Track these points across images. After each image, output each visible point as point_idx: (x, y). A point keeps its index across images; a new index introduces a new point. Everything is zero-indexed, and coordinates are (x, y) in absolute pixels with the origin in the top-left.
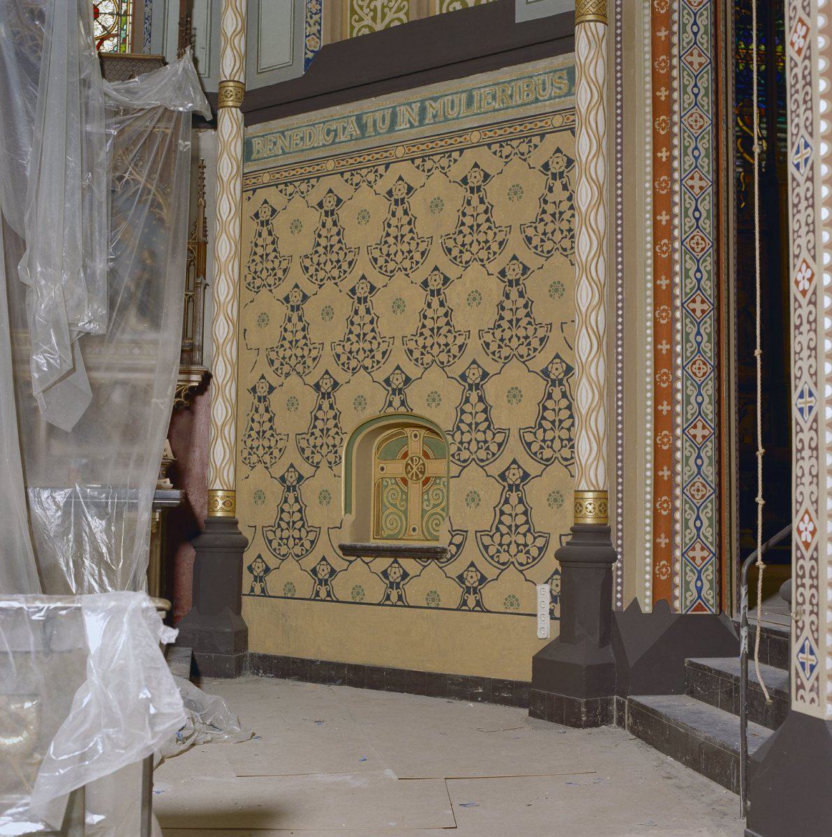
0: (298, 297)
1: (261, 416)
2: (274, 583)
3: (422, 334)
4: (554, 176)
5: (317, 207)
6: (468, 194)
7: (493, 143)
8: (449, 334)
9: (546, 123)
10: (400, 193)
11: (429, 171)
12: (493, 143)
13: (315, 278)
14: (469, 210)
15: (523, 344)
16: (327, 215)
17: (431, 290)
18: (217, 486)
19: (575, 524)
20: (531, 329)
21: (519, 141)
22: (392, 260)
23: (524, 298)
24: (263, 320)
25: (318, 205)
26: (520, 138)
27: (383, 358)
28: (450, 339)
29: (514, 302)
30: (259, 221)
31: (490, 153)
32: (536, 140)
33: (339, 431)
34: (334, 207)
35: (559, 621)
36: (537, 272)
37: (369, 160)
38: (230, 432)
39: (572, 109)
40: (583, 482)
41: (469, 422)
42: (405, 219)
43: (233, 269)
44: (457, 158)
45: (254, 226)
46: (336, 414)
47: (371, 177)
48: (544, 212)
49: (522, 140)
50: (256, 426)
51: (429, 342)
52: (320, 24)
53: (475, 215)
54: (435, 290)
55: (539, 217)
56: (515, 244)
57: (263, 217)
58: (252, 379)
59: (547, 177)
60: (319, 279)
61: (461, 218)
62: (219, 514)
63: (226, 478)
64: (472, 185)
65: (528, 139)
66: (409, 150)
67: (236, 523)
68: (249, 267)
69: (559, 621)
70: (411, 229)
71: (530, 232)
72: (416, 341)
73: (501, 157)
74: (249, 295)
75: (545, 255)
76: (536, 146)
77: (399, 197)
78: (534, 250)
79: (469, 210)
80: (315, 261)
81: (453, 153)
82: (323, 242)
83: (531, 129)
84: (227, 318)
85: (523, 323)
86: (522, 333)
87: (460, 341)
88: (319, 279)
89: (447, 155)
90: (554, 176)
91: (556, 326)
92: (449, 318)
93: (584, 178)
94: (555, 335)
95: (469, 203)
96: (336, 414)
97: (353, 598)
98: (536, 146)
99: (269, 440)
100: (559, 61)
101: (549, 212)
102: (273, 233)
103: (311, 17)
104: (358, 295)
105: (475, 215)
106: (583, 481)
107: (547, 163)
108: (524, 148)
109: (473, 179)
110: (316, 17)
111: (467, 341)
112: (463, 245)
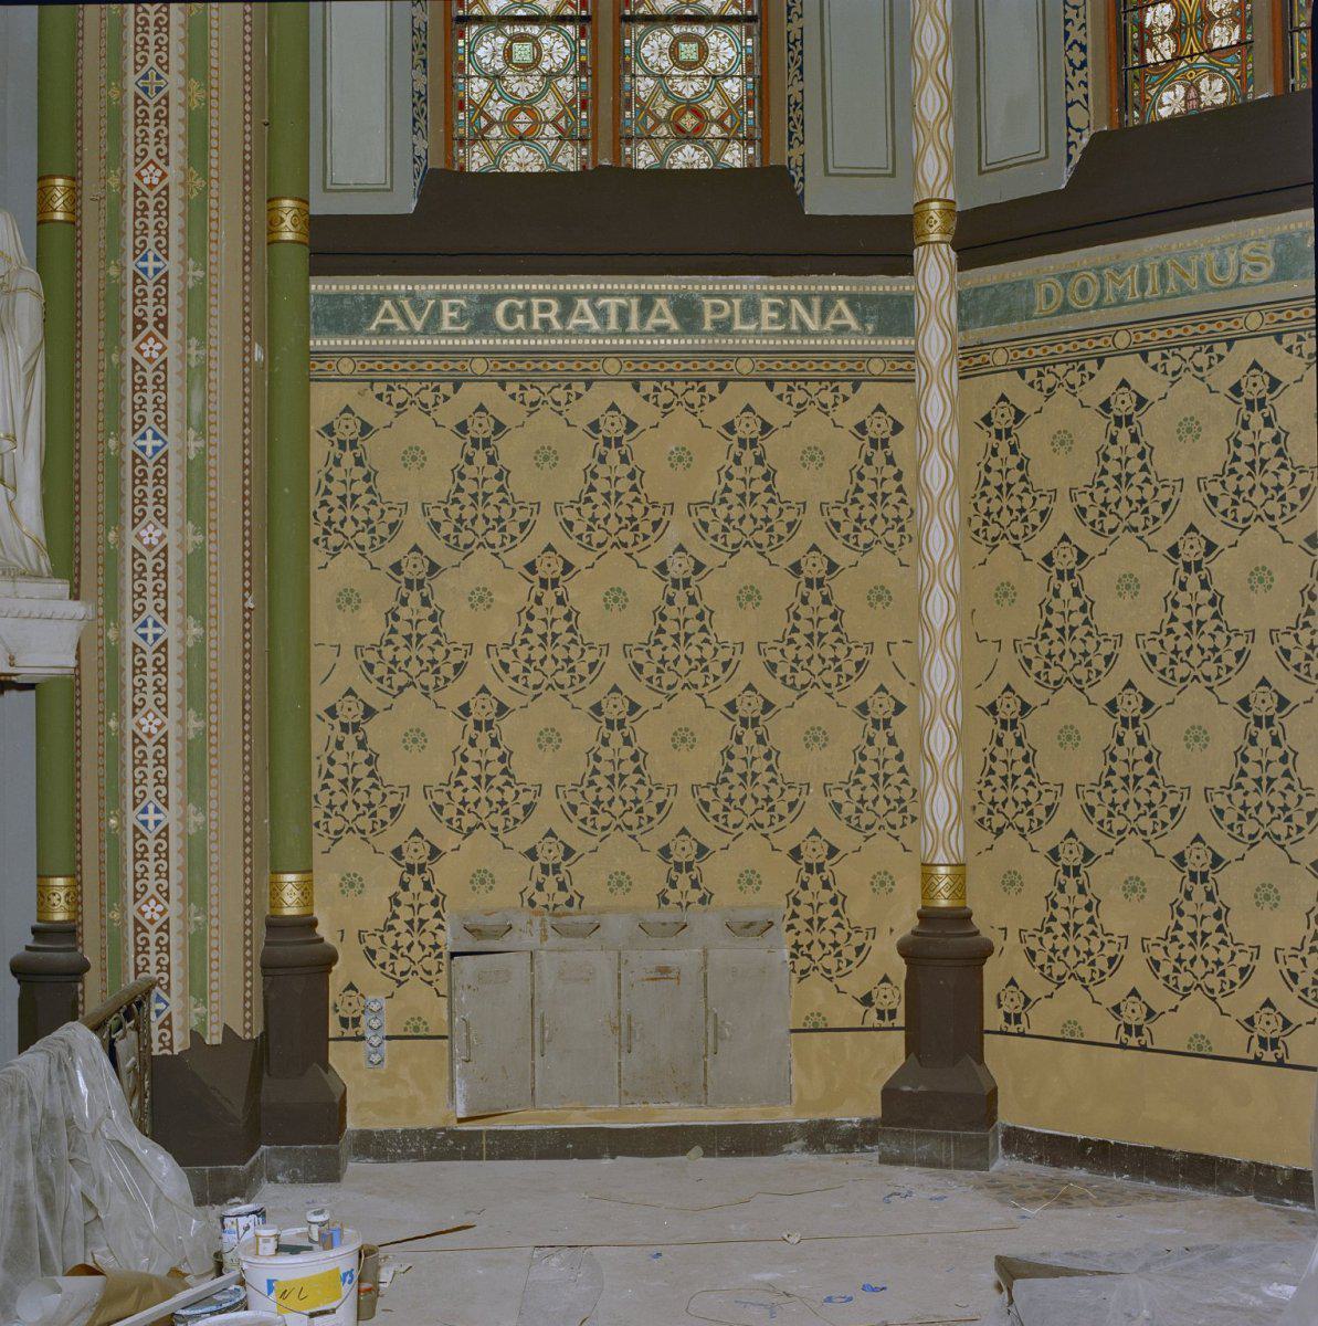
0: (1069, 555)
1: (1009, 752)
2: (1042, 1019)
3: (1045, 636)
4: (1118, 421)
5: (981, 423)
6: (993, 441)
7: (1286, 332)
8: (1088, 639)
9: (1236, 323)
10: (1003, 420)
11: (1174, 373)
12: (1286, 332)
13: (982, 535)
14: (995, 463)
15: (1209, 659)
16: (999, 436)
17: (1058, 571)
18: (941, 857)
19: (923, 907)
20: (1221, 638)
21: (1192, 349)
22: (1111, 513)
23: (1209, 589)
24: (1005, 593)
25: (983, 419)
26: (1194, 345)
27: (1237, 662)
28: (1091, 646)
29: (1194, 596)
30: (992, 430)
31: (1281, 349)
32: (1220, 348)
33: (1035, 781)
34: (1011, 423)
35: (985, 1028)
36: (848, 570)
37: (1022, 350)
38: (955, 773)
39: (910, 355)
40: (941, 851)
41: (1124, 775)
42: (1014, 461)
43: (952, 507)
44: (1224, 353)
45: (983, 438)
46: (1028, 754)
47: (1074, 377)
48: (1236, 458)
49: (1197, 348)
50: (1000, 769)
51: (1183, 644)
52: (1086, 85)
53: (879, 479)
54: (1192, 562)
55: (1228, 467)
56: (1192, 506)
57: (1000, 423)
58: (993, 691)
59: (1238, 407)
60: (989, 538)
61: (984, 474)
62: (943, 903)
63: (953, 845)
64: (999, 427)
65: (1078, 364)
66: (1016, 355)
67: (969, 916)
68: (976, 505)
69: (985, 1028)
70: (1145, 465)
71: (1084, 501)
72: (1037, 647)
73: (1165, 373)
74: (981, 550)
75: (990, 543)
76: (1221, 358)
77: (1003, 427)
78: (1222, 517)
79: (995, 463)
80: (1231, 487)
81: (1216, 346)
82: (995, 478)
83: (1196, 334)
84: (948, 589)
85: (1209, 627)
86: (1207, 642)
87: (1106, 649)
88: (989, 538)
89: (1205, 349)
90: (1118, 421)
91: (880, 648)
92: (1217, 608)
93: (935, 452)
94: (878, 658)
95: (994, 452)
96: (1028, 754)
97: (1062, 1032)
98: (1221, 358)
99: (1027, 791)
100: (880, 285)
101: (993, 484)
102: (1020, 451)
103: (1074, 74)
104: (1058, 566)
105: (879, 479)
106: (941, 851)
107: (1238, 384)
108: (1202, 359)
109: (1119, 405)
110: (1080, 75)
111: (868, 657)
112: (1105, 504)
